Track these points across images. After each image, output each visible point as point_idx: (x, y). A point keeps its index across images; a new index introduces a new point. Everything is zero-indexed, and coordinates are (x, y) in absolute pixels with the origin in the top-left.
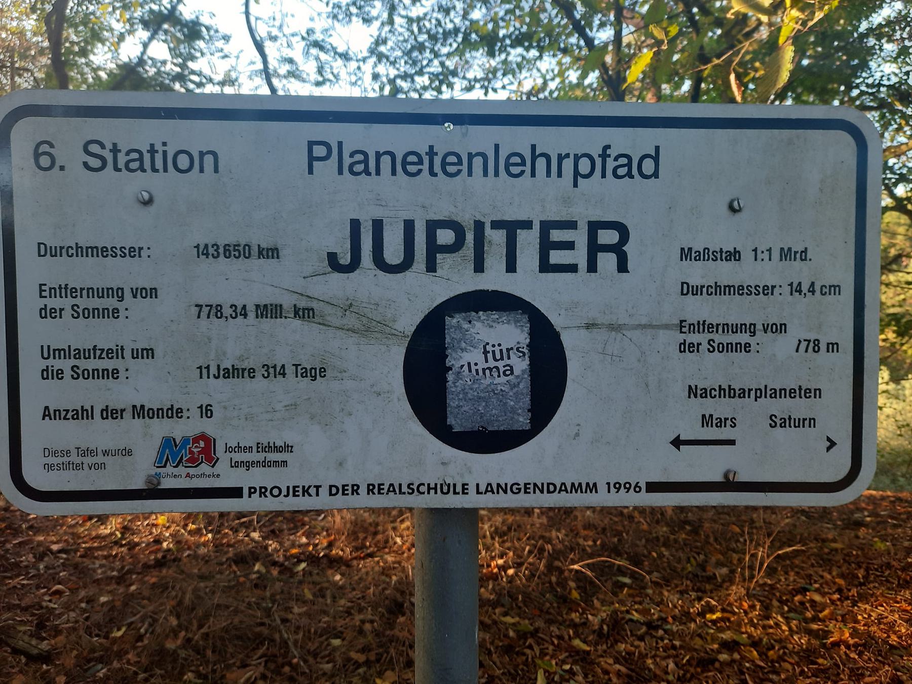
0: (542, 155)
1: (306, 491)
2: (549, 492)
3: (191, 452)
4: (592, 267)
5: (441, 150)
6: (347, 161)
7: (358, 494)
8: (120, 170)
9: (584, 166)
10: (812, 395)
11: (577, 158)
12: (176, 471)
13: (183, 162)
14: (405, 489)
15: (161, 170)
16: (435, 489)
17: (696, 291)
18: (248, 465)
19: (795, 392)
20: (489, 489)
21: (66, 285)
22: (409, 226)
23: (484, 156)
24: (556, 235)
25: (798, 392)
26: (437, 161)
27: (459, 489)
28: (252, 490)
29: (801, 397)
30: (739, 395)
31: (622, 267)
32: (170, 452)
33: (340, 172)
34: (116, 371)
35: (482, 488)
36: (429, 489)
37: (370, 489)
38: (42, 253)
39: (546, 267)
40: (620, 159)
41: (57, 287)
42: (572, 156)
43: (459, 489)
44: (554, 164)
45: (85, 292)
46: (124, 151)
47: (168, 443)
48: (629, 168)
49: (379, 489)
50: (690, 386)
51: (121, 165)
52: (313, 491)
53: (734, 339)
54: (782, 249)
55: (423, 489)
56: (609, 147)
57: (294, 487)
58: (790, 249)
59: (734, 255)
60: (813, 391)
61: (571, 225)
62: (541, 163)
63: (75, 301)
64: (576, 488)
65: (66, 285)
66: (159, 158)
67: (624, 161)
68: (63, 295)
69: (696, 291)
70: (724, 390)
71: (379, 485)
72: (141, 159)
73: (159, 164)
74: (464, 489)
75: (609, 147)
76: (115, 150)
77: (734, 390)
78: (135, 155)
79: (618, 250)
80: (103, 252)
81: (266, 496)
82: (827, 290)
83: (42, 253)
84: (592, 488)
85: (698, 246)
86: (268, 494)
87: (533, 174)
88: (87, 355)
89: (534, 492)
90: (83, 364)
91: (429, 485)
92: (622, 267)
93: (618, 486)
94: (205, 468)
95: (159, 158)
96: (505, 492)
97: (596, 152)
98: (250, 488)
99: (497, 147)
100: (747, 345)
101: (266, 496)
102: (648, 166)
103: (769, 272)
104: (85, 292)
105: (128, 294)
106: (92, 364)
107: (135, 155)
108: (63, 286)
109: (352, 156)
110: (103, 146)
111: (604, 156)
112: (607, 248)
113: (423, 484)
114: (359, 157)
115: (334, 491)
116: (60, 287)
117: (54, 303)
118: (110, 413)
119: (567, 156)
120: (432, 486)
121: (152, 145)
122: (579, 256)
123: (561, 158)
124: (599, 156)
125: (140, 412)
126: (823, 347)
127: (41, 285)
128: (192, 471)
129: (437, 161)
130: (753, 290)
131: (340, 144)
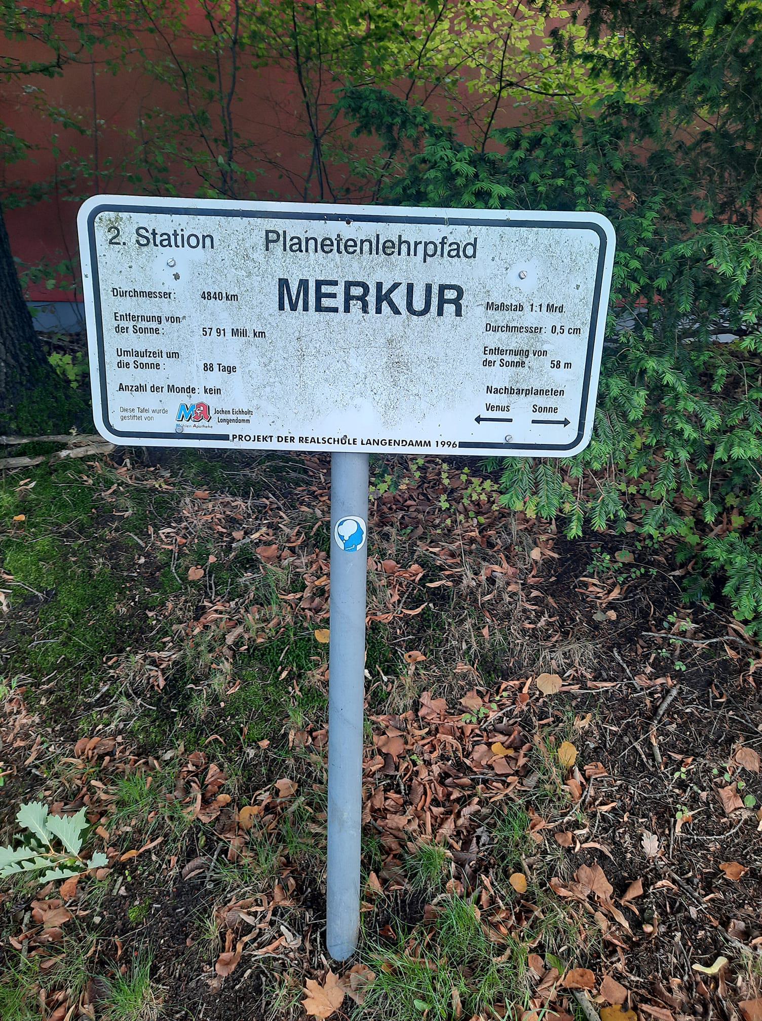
1: (264, 439)
3: (196, 413)
4: (347, 309)
5: (345, 237)
11: (426, 244)
13: (193, 241)
14: (320, 441)
18: (228, 421)
20: (369, 442)
22: (429, 288)
24: (325, 289)
27: (351, 442)
28: (234, 437)
31: (458, 313)
32: (186, 413)
34: (158, 365)
35: (365, 442)
39: (319, 308)
47: (184, 407)
48: (458, 251)
51: (158, 242)
61: (335, 283)
62: (404, 248)
66: (179, 238)
72: (169, 239)
73: (179, 243)
76: (154, 234)
78: (165, 237)
79: (457, 302)
80: (150, 295)
84: (429, 444)
87: (399, 254)
90: (140, 360)
92: (458, 313)
94: (204, 422)
95: (179, 238)
99: (378, 236)
100: (157, 329)
106: (145, 360)
107: (165, 237)
109: (291, 240)
110: (147, 231)
111: (443, 243)
112: (450, 301)
114: (296, 241)
118: (155, 389)
119: (421, 243)
121: (175, 231)
122: (339, 302)
123: (416, 244)
125: (171, 389)
126: (562, 365)
131: (285, 232)
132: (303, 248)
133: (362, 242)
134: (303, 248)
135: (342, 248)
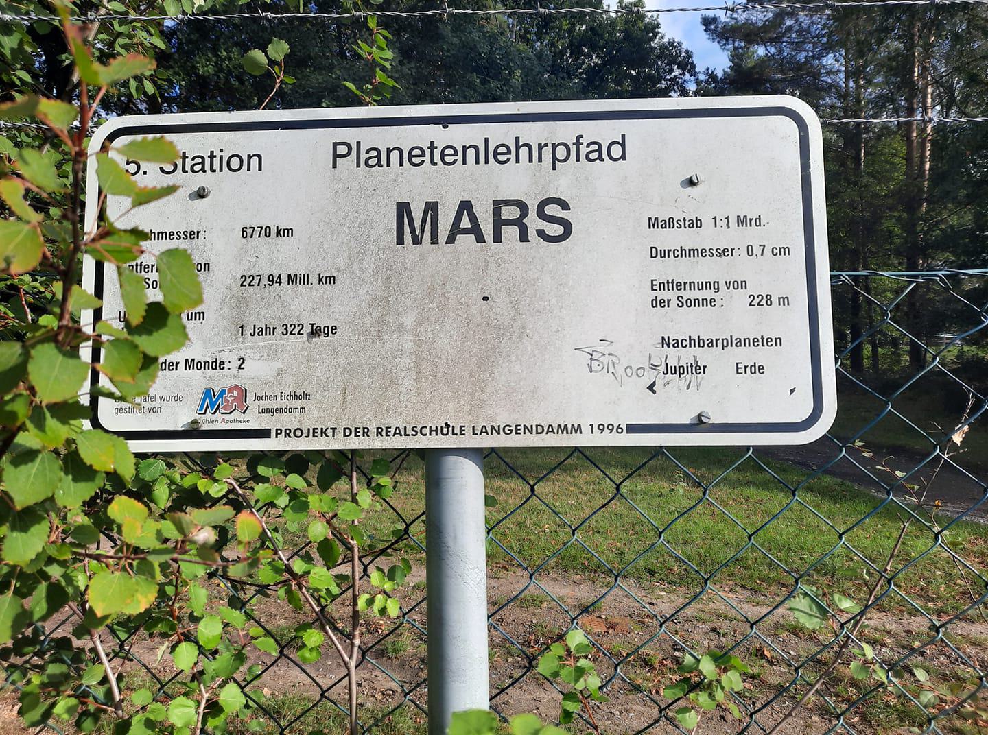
0: (523, 145)
2: (537, 433)
6: (363, 157)
7: (368, 436)
8: (187, 172)
9: (561, 153)
10: (774, 342)
12: (214, 417)
14: (410, 432)
15: (218, 170)
16: (436, 431)
17: (665, 254)
18: (272, 412)
19: (758, 341)
21: (673, 280)
23: (476, 148)
25: (760, 340)
26: (437, 153)
27: (457, 431)
29: (763, 345)
30: (708, 344)
32: (211, 400)
33: (358, 166)
36: (431, 431)
37: (379, 432)
38: (654, 255)
40: (591, 146)
41: (665, 282)
42: (550, 145)
43: (457, 431)
44: (536, 152)
45: (688, 286)
46: (190, 158)
49: (387, 432)
50: (663, 337)
51: (188, 168)
52: (329, 432)
53: (700, 296)
54: (738, 217)
55: (426, 431)
56: (581, 136)
57: (314, 429)
58: (745, 217)
59: (696, 223)
60: (774, 340)
62: (524, 152)
63: (680, 293)
64: (563, 429)
65: (673, 280)
66: (216, 161)
67: (595, 147)
68: (670, 288)
69: (665, 254)
70: (694, 340)
71: (387, 428)
72: (203, 163)
74: (461, 431)
75: (581, 136)
77: (703, 340)
81: (290, 437)
82: (778, 251)
83: (654, 255)
84: (578, 429)
85: (663, 217)
86: (292, 434)
87: (517, 161)
88: (747, 341)
89: (525, 433)
91: (430, 427)
93: (601, 428)
96: (498, 433)
97: (570, 141)
98: (277, 430)
99: (486, 140)
101: (290, 437)
102: (616, 151)
103: (736, 237)
104: (688, 286)
105: (722, 286)
108: (670, 281)
111: (578, 143)
113: (426, 427)
115: (347, 432)
116: (668, 282)
117: (663, 295)
119: (546, 145)
120: (434, 428)
121: (212, 152)
123: (540, 147)
124: (574, 144)
127: (652, 281)
128: (227, 417)
129: (437, 153)
130: (182, 235)
131: (358, 143)
132: (384, 162)
133: (389, 151)
134: (384, 162)
135: (437, 159)
